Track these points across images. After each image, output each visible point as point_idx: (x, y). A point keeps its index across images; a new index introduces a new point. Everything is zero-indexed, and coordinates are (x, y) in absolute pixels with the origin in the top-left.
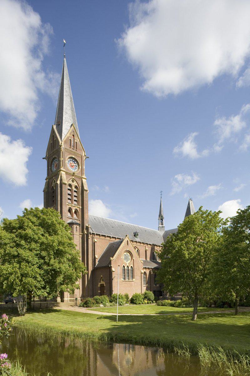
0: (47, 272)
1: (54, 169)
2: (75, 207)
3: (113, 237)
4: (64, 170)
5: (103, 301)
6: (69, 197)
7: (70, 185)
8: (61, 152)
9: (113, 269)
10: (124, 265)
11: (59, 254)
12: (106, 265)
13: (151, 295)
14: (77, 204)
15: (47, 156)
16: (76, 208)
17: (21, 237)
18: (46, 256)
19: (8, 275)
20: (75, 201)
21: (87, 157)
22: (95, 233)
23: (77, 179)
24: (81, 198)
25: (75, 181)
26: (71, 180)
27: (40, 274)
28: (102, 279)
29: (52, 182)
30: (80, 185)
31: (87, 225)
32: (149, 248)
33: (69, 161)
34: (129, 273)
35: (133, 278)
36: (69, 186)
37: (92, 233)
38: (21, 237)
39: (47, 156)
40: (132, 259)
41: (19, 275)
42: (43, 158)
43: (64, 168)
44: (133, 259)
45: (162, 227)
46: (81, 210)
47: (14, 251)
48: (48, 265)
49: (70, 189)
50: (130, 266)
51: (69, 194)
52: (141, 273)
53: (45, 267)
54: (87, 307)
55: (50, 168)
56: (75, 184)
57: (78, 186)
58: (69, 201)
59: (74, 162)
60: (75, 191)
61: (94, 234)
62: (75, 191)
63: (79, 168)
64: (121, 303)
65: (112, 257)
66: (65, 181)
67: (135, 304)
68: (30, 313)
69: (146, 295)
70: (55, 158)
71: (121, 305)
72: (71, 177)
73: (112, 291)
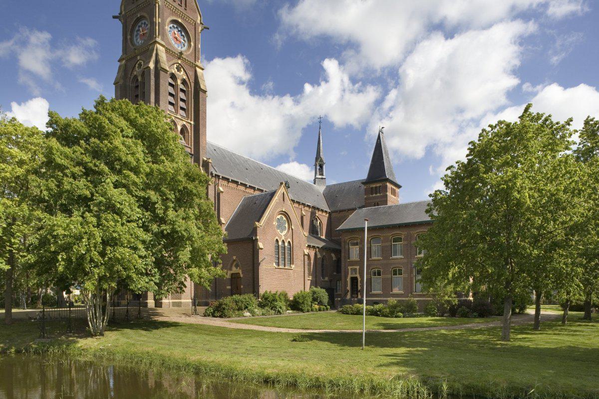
0: (160, 235)
1: (139, 41)
2: (183, 120)
3: (251, 187)
4: (163, 43)
5: (248, 304)
6: (171, 99)
7: (173, 76)
8: (157, 5)
9: (261, 245)
10: (277, 238)
11: (184, 199)
12: (246, 236)
13: (323, 294)
14: (185, 115)
15: (123, 13)
16: (185, 123)
17: (96, 154)
18: (157, 203)
19: (69, 240)
20: (182, 108)
21: (205, 28)
22: (221, 175)
23: (186, 67)
24: (193, 106)
25: (182, 69)
26: (175, 66)
27: (144, 242)
28: (235, 263)
29: (135, 66)
30: (192, 80)
31: (205, 159)
32: (306, 212)
33: (170, 28)
34: (285, 254)
35: (291, 264)
36: (171, 77)
37: (216, 175)
38: (96, 154)
39: (123, 13)
40: (290, 229)
41: (99, 240)
42: (114, 17)
43: (163, 40)
44: (292, 229)
45: (322, 178)
46: (193, 129)
47: (82, 187)
48: (162, 221)
49: (174, 83)
50: (287, 242)
51: (171, 94)
52: (305, 255)
53: (155, 227)
54: (221, 317)
55: (129, 37)
56: (181, 75)
57: (187, 80)
58: (170, 107)
59: (181, 33)
60: (182, 90)
61: (219, 176)
62: (182, 90)
63: (190, 46)
64: (280, 309)
65: (258, 221)
66: (165, 63)
67: (302, 310)
68: (112, 331)
69: (315, 296)
70: (142, 17)
71: (280, 313)
72: (175, 61)
73: (258, 286)
